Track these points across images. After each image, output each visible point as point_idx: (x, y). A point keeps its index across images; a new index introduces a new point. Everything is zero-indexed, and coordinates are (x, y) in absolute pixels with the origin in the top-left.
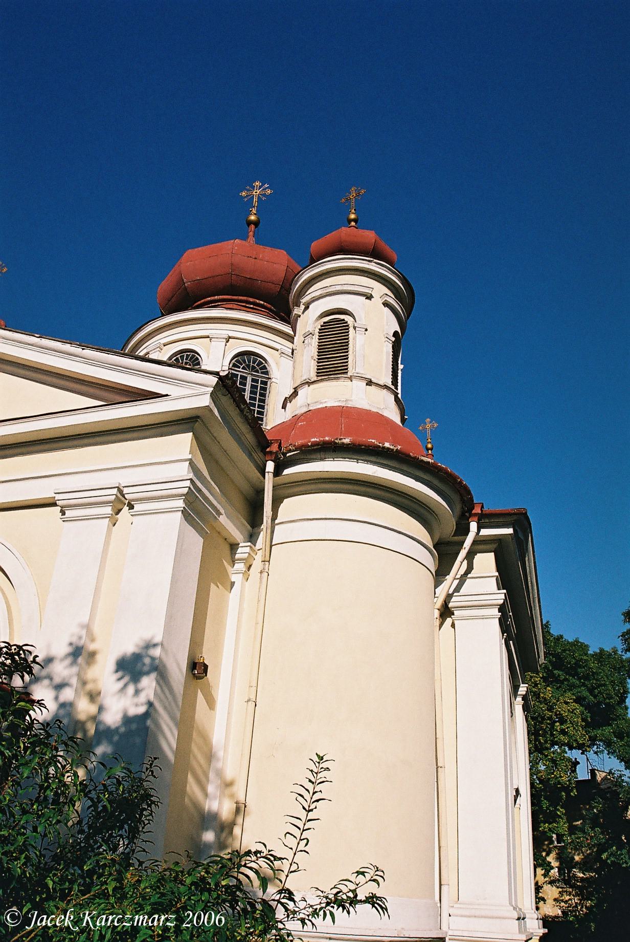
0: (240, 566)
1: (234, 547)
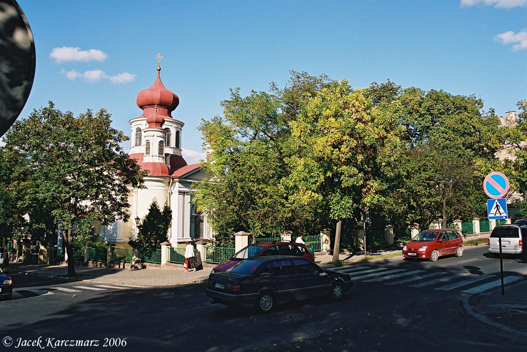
0: (134, 192)
1: (133, 190)
